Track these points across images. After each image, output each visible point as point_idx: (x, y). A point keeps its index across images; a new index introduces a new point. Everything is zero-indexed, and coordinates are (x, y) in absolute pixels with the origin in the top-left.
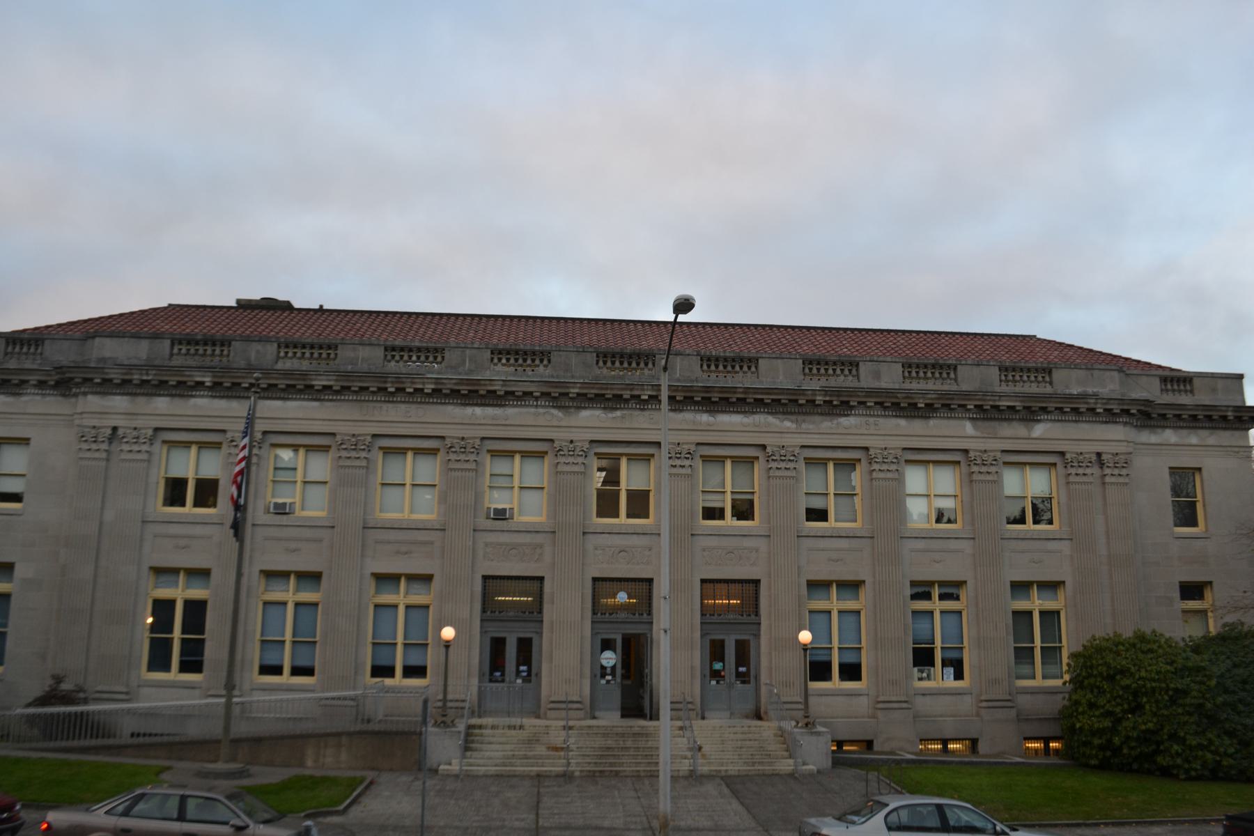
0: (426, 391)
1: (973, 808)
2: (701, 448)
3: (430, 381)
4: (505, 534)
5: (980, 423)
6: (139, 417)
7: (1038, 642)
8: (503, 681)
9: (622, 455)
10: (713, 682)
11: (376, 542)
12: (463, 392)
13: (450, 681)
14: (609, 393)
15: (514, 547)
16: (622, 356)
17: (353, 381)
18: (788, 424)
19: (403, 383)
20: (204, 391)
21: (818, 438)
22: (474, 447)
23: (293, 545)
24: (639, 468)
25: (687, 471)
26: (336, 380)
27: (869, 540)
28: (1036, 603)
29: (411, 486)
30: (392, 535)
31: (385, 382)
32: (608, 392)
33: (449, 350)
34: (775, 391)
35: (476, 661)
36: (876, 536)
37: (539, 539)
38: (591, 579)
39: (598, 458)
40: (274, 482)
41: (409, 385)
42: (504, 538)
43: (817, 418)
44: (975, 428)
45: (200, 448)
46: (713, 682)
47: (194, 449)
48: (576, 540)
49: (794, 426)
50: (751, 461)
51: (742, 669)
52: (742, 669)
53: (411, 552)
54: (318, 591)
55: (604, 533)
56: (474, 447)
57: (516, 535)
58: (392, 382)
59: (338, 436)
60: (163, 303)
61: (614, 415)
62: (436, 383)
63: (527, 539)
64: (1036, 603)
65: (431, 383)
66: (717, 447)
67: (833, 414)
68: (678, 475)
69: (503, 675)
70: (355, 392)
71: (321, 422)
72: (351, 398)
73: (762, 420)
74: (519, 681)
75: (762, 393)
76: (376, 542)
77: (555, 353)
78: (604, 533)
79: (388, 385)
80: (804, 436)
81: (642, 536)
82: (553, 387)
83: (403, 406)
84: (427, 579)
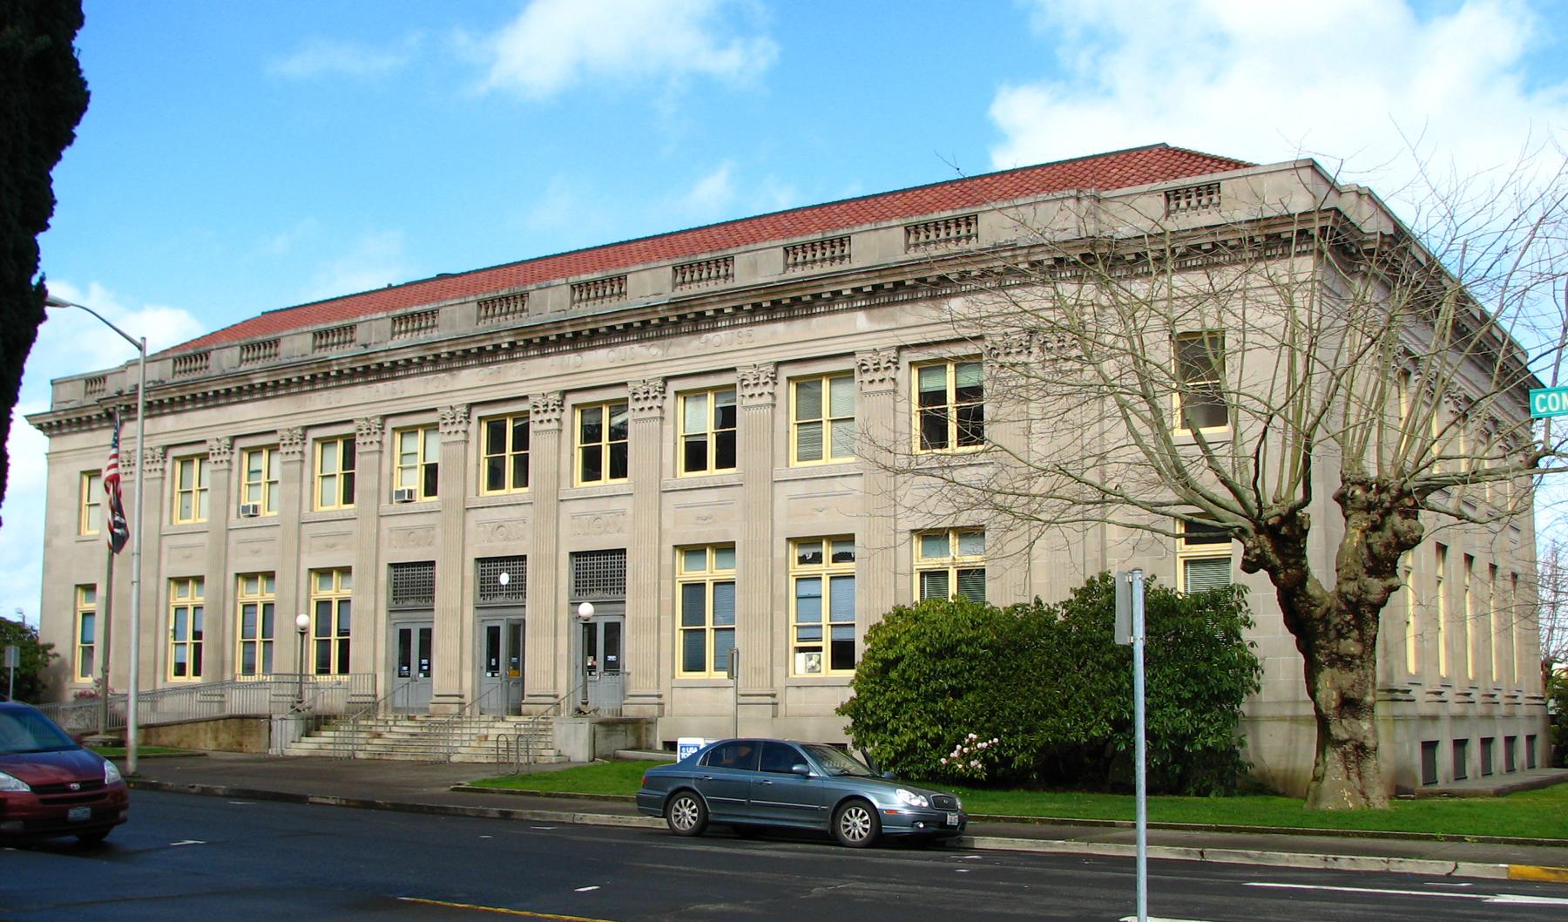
1: (566, 816)
2: (904, 354)
5: (876, 312)
6: (156, 437)
7: (709, 624)
8: (409, 676)
9: (821, 375)
10: (489, 674)
12: (618, 328)
14: (585, 329)
16: (515, 297)
17: (502, 337)
18: (654, 351)
20: (618, 337)
22: (890, 361)
23: (331, 541)
24: (842, 390)
25: (888, 386)
27: (858, 478)
28: (709, 571)
29: (829, 423)
34: (624, 314)
35: (381, 654)
38: (568, 554)
40: (402, 468)
42: (256, 534)
43: (685, 339)
44: (870, 319)
45: (402, 435)
46: (489, 674)
47: (265, 453)
49: (660, 353)
51: (611, 658)
52: (611, 658)
54: (734, 567)
56: (890, 361)
59: (857, 355)
60: (256, 313)
64: (709, 571)
65: (509, 336)
66: (520, 402)
67: (697, 331)
68: (546, 431)
69: (409, 669)
70: (974, 278)
72: (757, 319)
73: (628, 352)
74: (422, 675)
75: (612, 319)
80: (668, 363)
82: (425, 350)
83: (325, 393)
84: (346, 571)
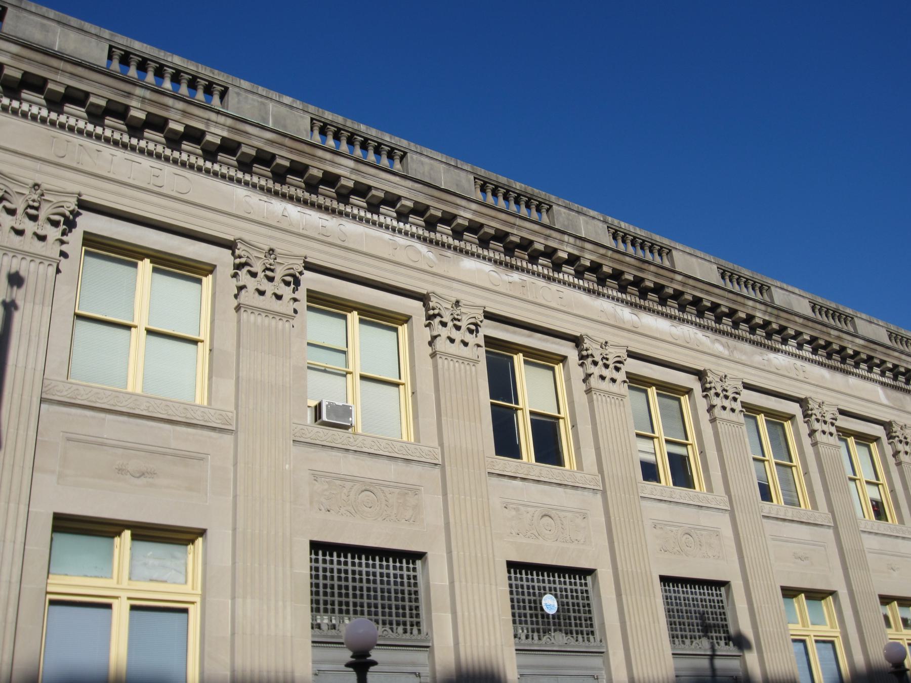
0: (209, 138)
3: (221, 119)
4: (351, 457)
11: (69, 439)
13: (76, 443)
15: (369, 487)
19: (166, 107)
21: (754, 375)
26: (16, 56)
30: (112, 427)
31: (129, 95)
32: (515, 232)
33: (238, 94)
36: (406, 378)
37: (412, 474)
39: (155, 270)
41: (178, 117)
48: (769, 647)
50: (669, 391)
53: (152, 474)
55: (515, 478)
57: (369, 461)
58: (143, 99)
61: (510, 279)
62: (231, 129)
63: (390, 472)
71: (40, 366)
76: (69, 439)
77: (415, 156)
78: (515, 478)
79: (134, 103)
81: (569, 491)
